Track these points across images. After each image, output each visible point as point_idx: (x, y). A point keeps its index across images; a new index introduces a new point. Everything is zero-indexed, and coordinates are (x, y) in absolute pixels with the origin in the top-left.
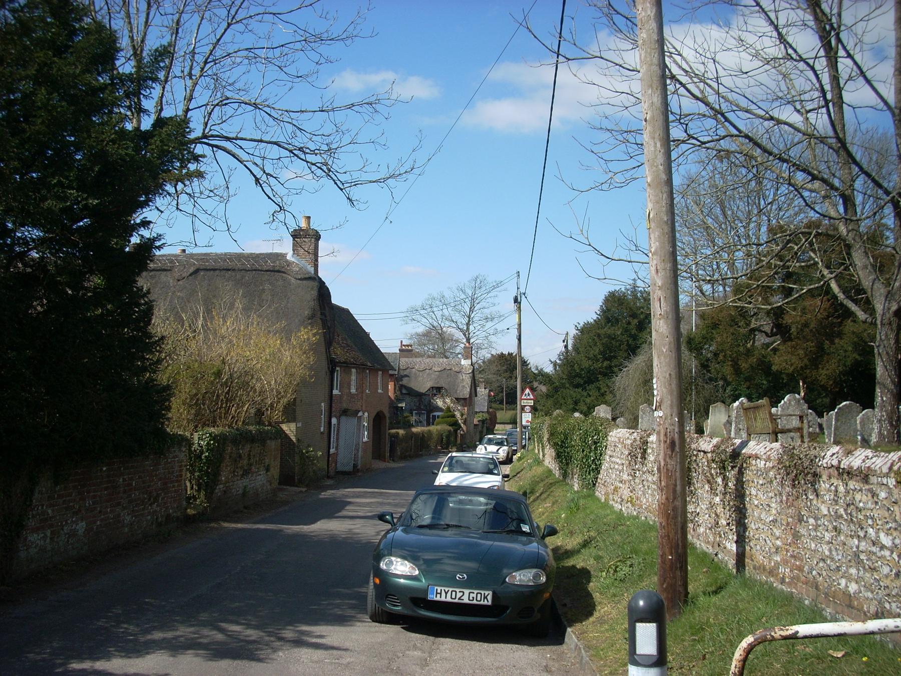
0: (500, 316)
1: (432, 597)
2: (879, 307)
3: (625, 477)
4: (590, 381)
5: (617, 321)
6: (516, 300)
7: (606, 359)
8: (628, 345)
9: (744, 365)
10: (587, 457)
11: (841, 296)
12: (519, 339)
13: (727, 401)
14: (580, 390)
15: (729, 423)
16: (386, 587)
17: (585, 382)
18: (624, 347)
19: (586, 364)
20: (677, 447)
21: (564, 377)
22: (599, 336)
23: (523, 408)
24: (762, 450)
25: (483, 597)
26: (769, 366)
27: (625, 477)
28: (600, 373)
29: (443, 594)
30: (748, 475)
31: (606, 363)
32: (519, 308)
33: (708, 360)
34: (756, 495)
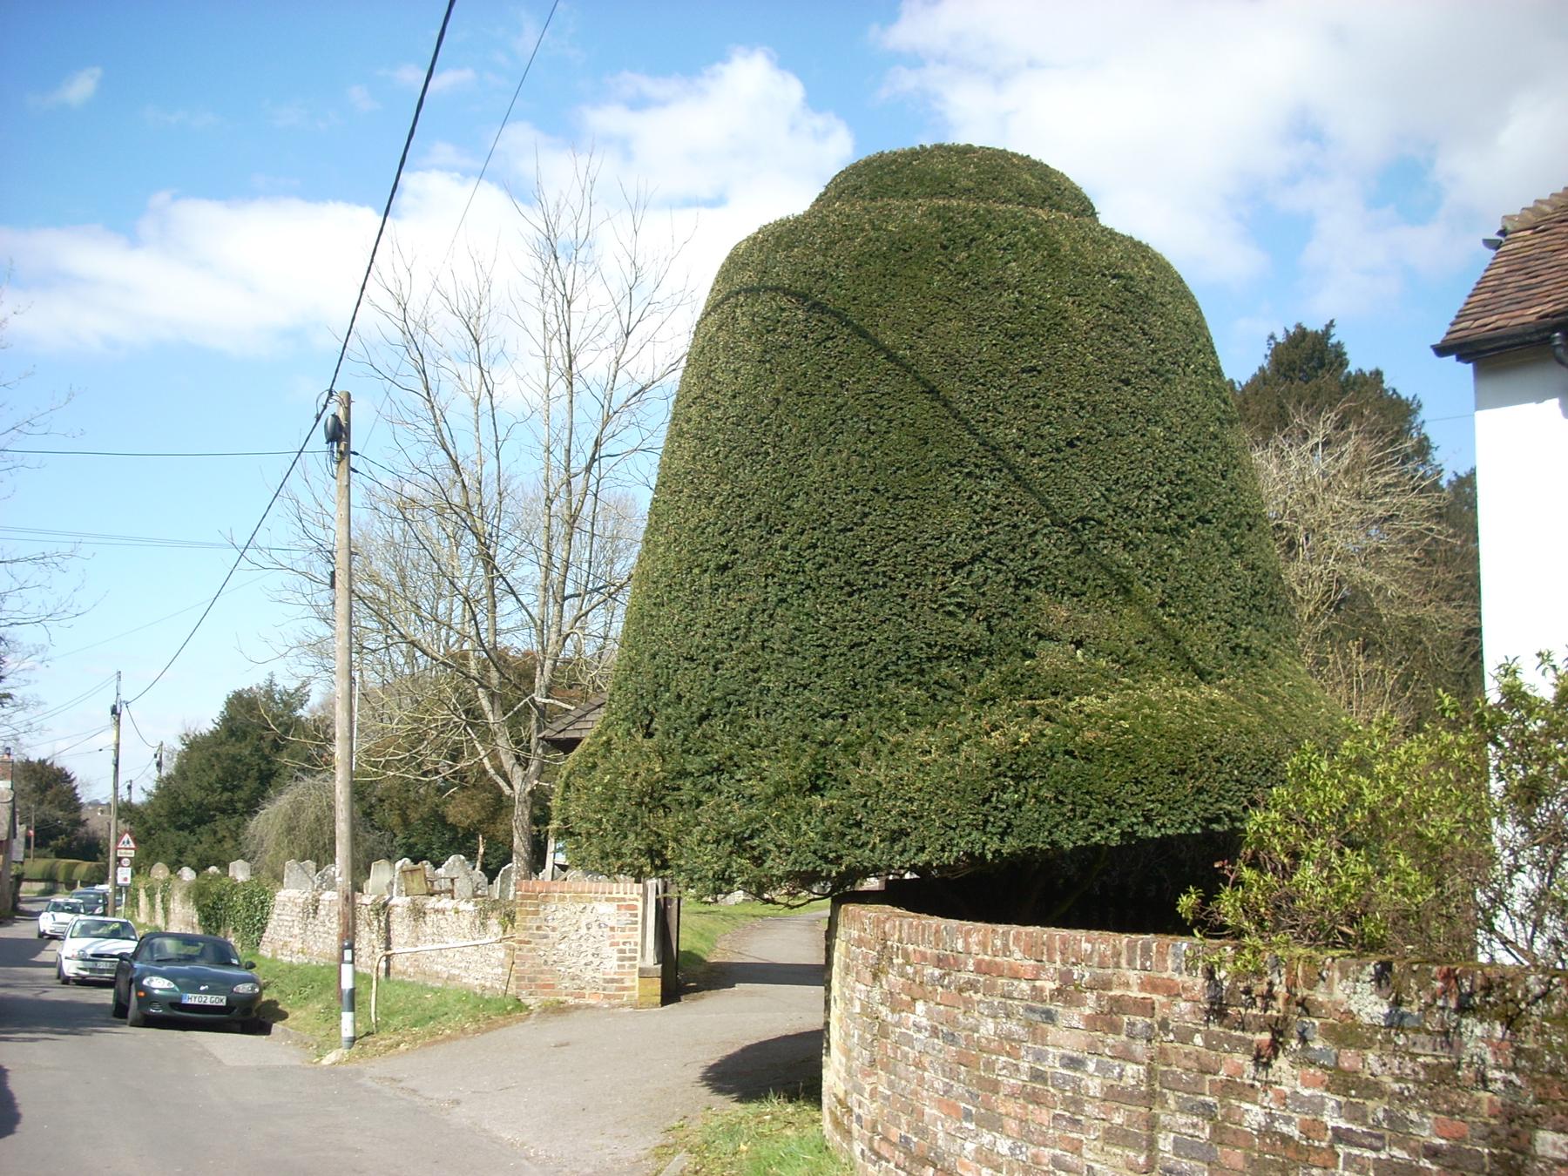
0: (39, 703)
1: (185, 1001)
2: (517, 787)
3: (296, 931)
4: (200, 821)
5: (245, 735)
6: (114, 711)
7: (225, 789)
8: (260, 771)
9: (414, 816)
10: (251, 917)
11: (492, 772)
12: (116, 765)
13: (391, 857)
14: (186, 833)
15: (392, 883)
16: (149, 998)
17: (194, 822)
18: (254, 773)
19: (197, 796)
20: (350, 900)
21: (163, 813)
22: (218, 756)
23: (119, 859)
24: (400, 902)
25: (220, 1000)
26: (442, 819)
27: (296, 931)
28: (217, 809)
29: (192, 999)
30: (392, 917)
31: (226, 795)
32: (118, 722)
33: (371, 806)
34: (397, 928)
